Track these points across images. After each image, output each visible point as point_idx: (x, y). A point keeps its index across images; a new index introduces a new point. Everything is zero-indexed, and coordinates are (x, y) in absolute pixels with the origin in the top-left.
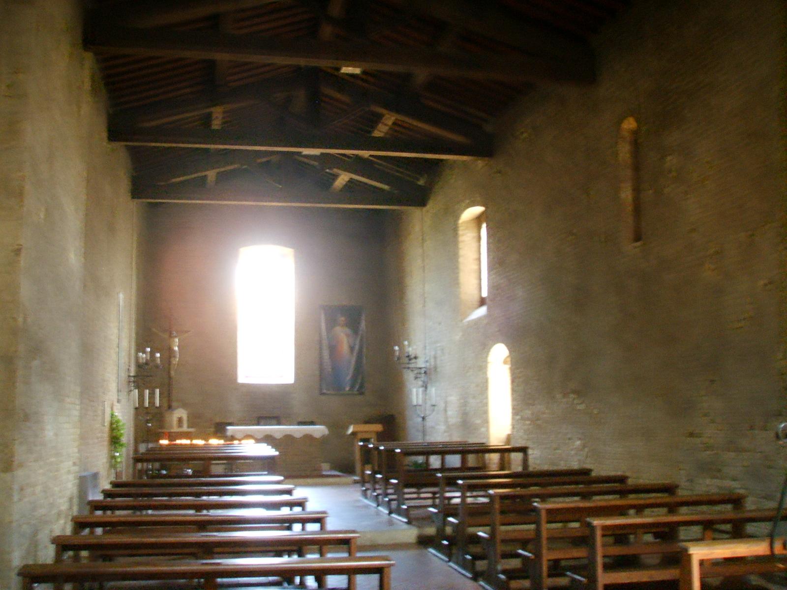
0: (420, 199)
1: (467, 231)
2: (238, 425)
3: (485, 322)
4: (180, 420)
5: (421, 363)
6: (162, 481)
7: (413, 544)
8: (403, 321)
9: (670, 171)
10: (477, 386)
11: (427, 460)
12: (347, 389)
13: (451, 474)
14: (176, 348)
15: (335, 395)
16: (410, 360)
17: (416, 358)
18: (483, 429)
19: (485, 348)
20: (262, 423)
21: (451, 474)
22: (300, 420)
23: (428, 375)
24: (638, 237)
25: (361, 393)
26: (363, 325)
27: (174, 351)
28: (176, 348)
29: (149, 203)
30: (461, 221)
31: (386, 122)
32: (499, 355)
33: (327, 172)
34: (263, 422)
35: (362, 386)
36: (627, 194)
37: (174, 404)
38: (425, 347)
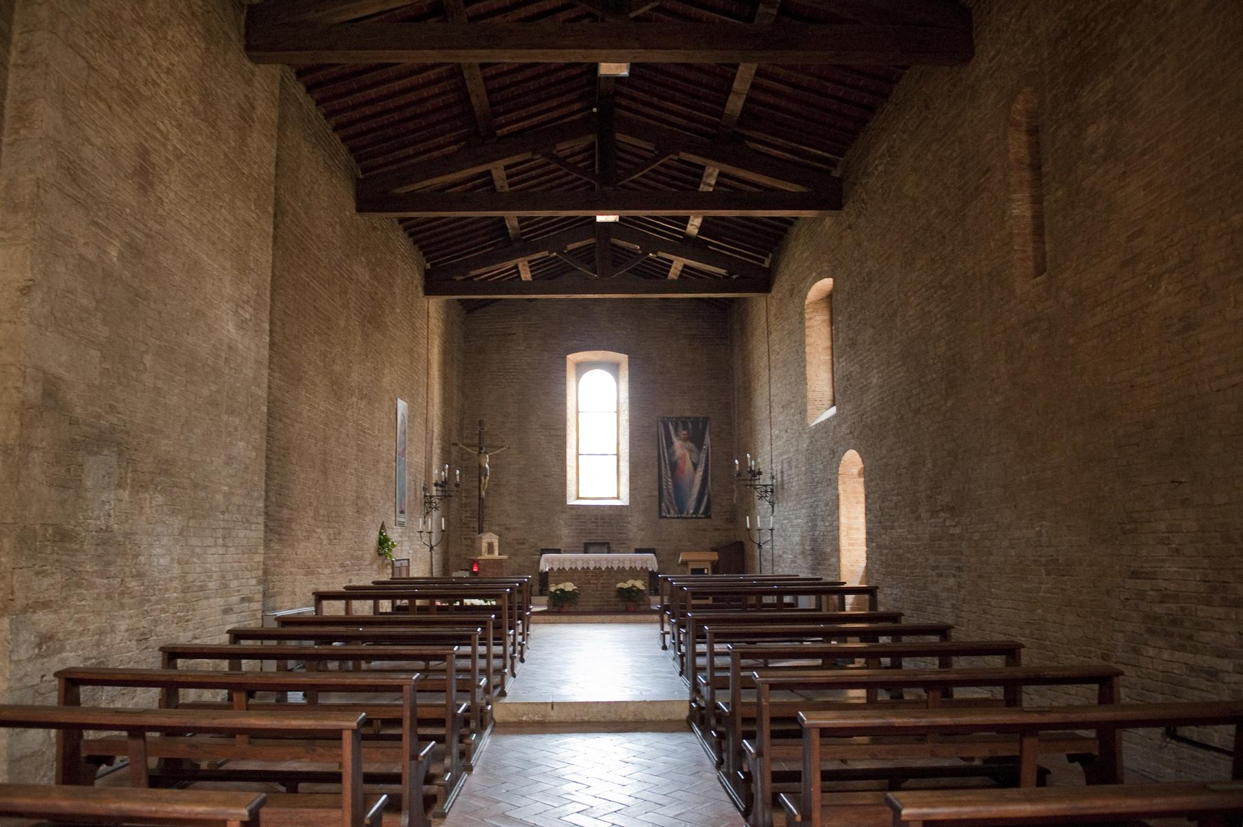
0: (764, 284)
1: (814, 314)
2: (565, 552)
3: (834, 423)
4: (490, 546)
5: (765, 479)
6: (435, 617)
7: (680, 721)
8: (752, 432)
9: (1093, 149)
10: (827, 505)
11: (797, 600)
12: (691, 511)
13: (416, 630)
14: (487, 466)
15: (678, 518)
16: (755, 476)
17: (760, 473)
18: (833, 560)
19: (835, 456)
20: (591, 551)
21: (416, 630)
22: (637, 546)
23: (774, 493)
24: (1040, 269)
25: (708, 517)
26: (707, 440)
27: (486, 468)
28: (487, 466)
29: (459, 300)
30: (807, 302)
31: (708, 181)
32: (852, 461)
33: (650, 259)
34: (592, 549)
35: (708, 508)
36: (1021, 209)
37: (486, 526)
38: (772, 460)
